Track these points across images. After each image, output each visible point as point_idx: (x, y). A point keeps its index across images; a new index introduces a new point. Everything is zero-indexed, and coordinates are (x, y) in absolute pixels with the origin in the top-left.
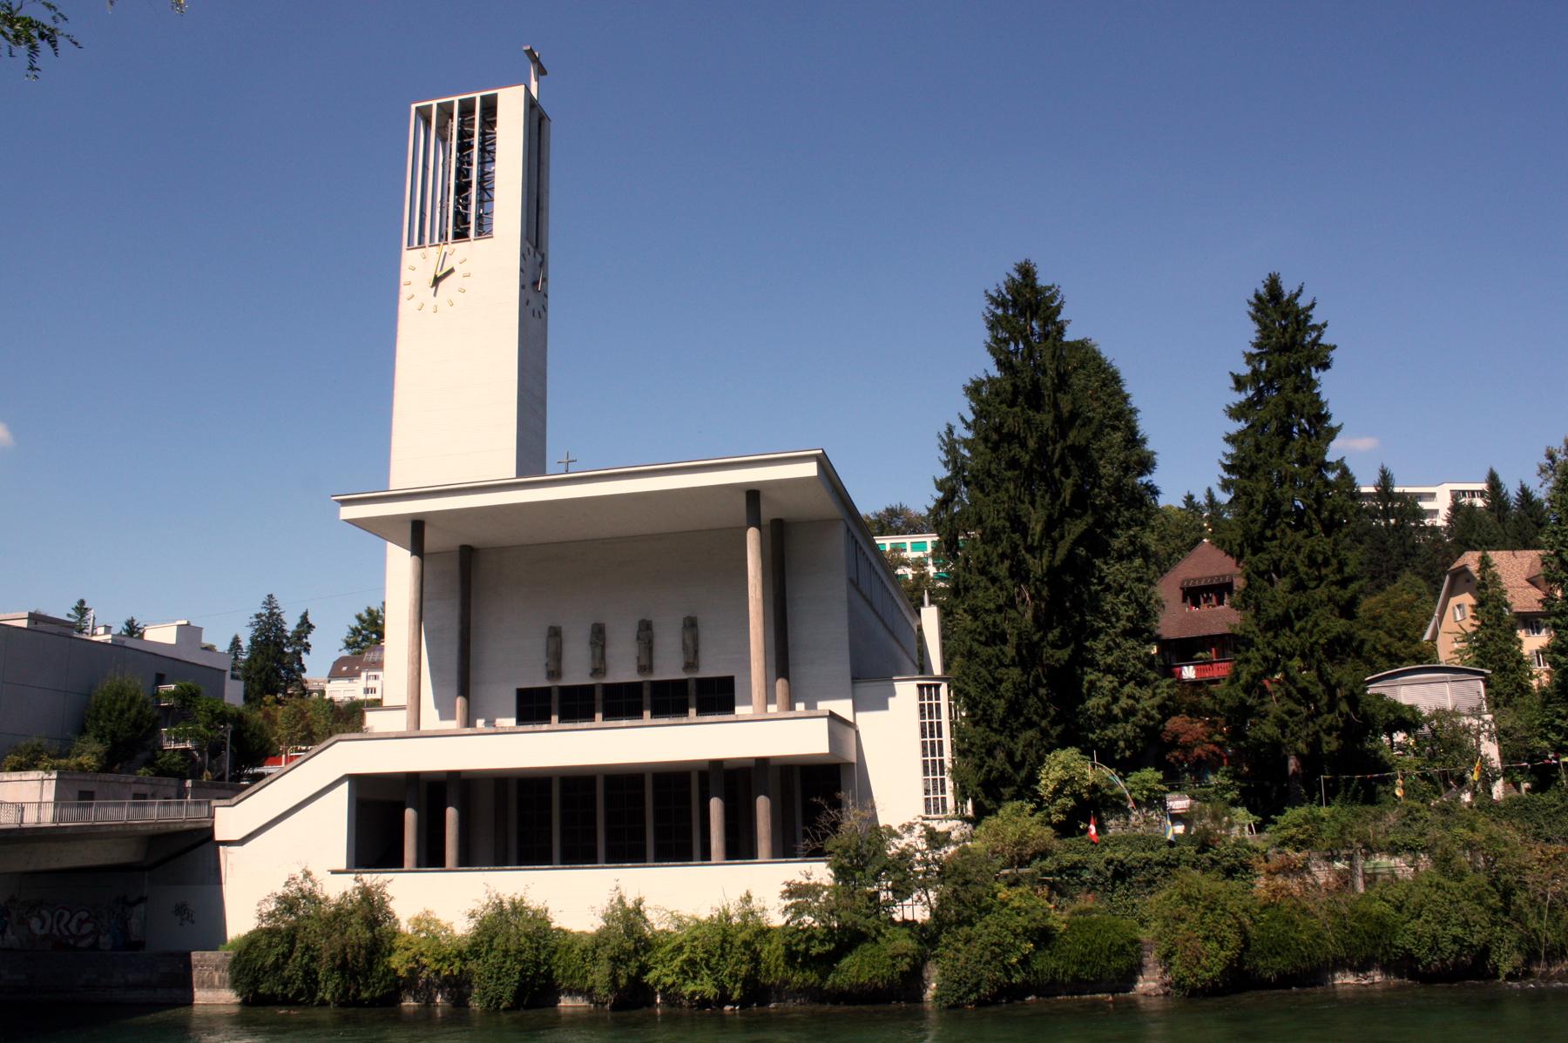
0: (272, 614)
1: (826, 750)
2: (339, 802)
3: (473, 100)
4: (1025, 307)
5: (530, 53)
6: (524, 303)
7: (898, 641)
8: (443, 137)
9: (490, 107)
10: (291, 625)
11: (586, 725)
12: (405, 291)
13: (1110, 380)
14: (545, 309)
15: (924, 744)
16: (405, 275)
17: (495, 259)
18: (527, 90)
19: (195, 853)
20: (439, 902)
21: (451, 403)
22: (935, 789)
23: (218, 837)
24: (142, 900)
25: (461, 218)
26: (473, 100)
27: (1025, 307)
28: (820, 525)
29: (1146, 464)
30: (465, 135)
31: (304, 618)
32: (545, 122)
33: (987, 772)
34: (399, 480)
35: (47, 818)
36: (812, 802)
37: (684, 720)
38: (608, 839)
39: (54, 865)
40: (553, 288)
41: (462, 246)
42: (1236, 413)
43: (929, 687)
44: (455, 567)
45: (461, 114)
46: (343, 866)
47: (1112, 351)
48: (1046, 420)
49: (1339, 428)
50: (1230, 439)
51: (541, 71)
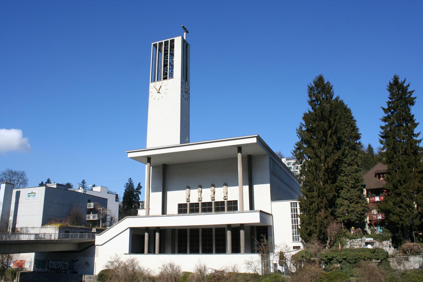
0: (131, 183)
1: (259, 222)
2: (127, 235)
3: (168, 41)
4: (320, 90)
5: (183, 27)
6: (182, 96)
7: (293, 190)
8: (160, 50)
9: (172, 41)
10: (136, 186)
11: (209, 213)
12: (150, 94)
13: (347, 111)
14: (189, 98)
15: (292, 220)
16: (151, 90)
17: (174, 84)
18: (183, 38)
19: (88, 248)
20: (152, 263)
21: (163, 125)
22: (296, 234)
23: (96, 244)
24: (77, 260)
25: (165, 74)
26: (168, 41)
27: (320, 90)
28: (261, 156)
29: (358, 137)
30: (166, 50)
31: (139, 184)
32: (188, 46)
33: (309, 229)
34: (148, 146)
35: (57, 238)
36: (258, 236)
37: (186, 214)
38: (203, 247)
39: (53, 250)
40: (191, 92)
41: (165, 81)
42: (385, 120)
43: (294, 203)
44: (161, 170)
45: (165, 45)
46: (128, 253)
47: (349, 103)
48: (327, 123)
49: (418, 124)
50: (382, 128)
51: (187, 32)
